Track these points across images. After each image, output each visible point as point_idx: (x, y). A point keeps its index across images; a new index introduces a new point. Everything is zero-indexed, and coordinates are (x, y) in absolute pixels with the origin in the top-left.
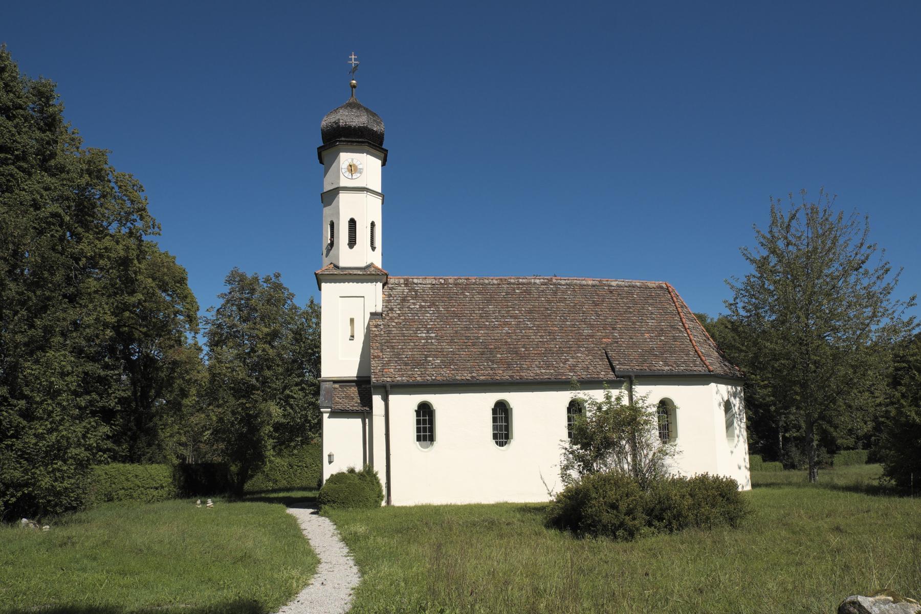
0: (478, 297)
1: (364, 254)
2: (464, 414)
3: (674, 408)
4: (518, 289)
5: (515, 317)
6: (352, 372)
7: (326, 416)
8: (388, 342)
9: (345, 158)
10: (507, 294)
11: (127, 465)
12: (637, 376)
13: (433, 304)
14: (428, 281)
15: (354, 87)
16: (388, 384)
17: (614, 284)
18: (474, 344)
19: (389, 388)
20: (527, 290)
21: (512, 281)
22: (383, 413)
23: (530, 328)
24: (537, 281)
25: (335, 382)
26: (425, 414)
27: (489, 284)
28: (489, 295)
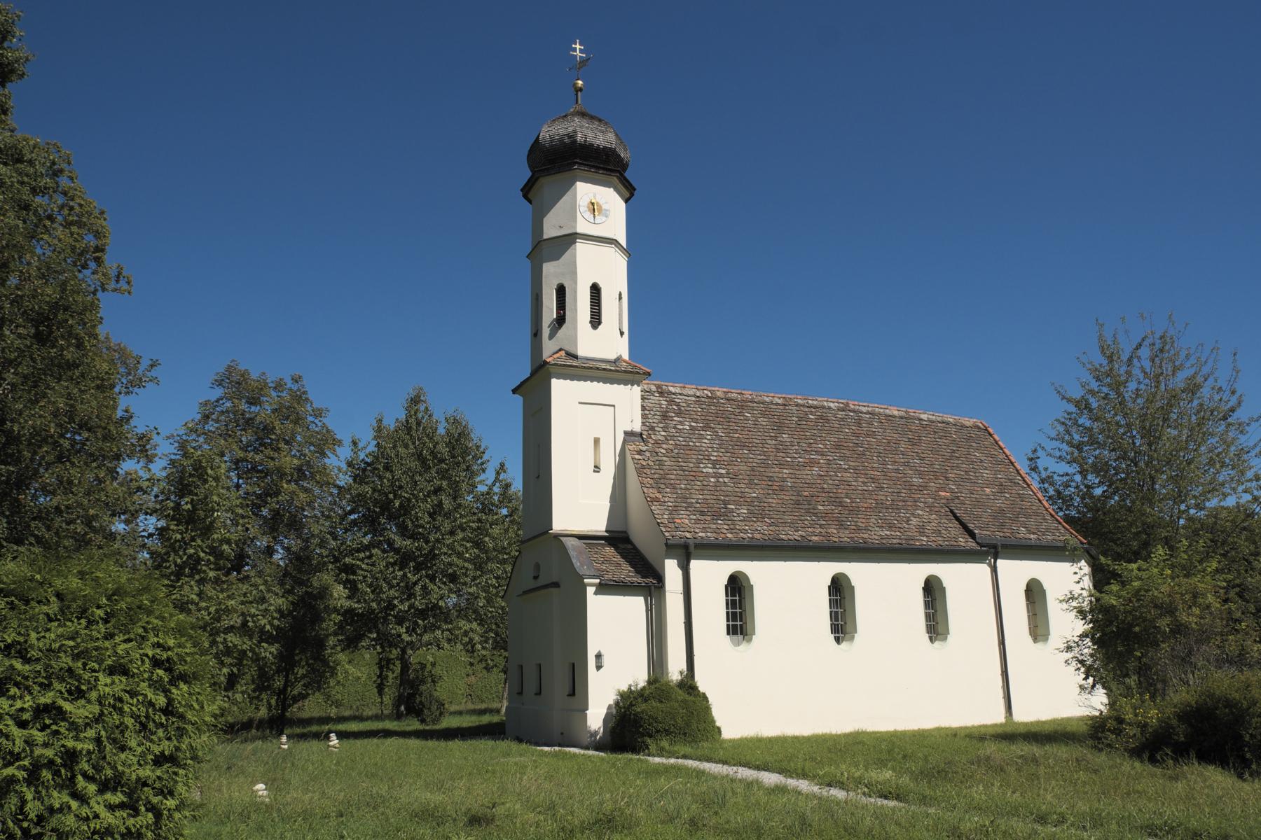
0: (763, 421)
1: (606, 341)
2: (789, 590)
3: (1043, 592)
6: (597, 523)
7: (590, 591)
9: (585, 192)
10: (800, 419)
12: (1005, 546)
15: (581, 90)
16: (691, 542)
17: (924, 417)
19: (692, 549)
20: (823, 416)
24: (832, 405)
25: (581, 537)
26: (737, 588)
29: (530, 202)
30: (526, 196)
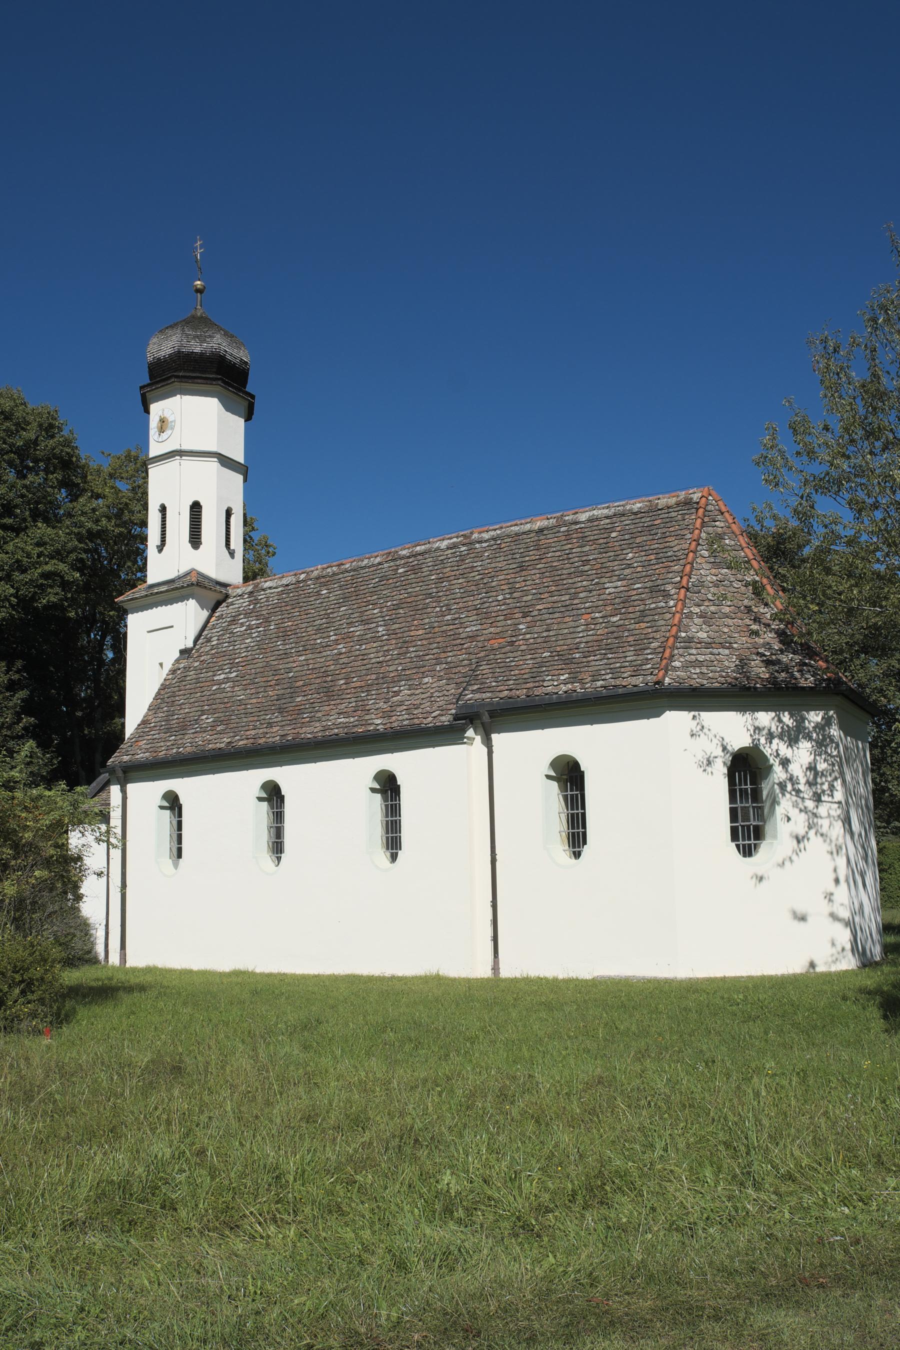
14: (285, 581)
15: (199, 291)
21: (404, 552)
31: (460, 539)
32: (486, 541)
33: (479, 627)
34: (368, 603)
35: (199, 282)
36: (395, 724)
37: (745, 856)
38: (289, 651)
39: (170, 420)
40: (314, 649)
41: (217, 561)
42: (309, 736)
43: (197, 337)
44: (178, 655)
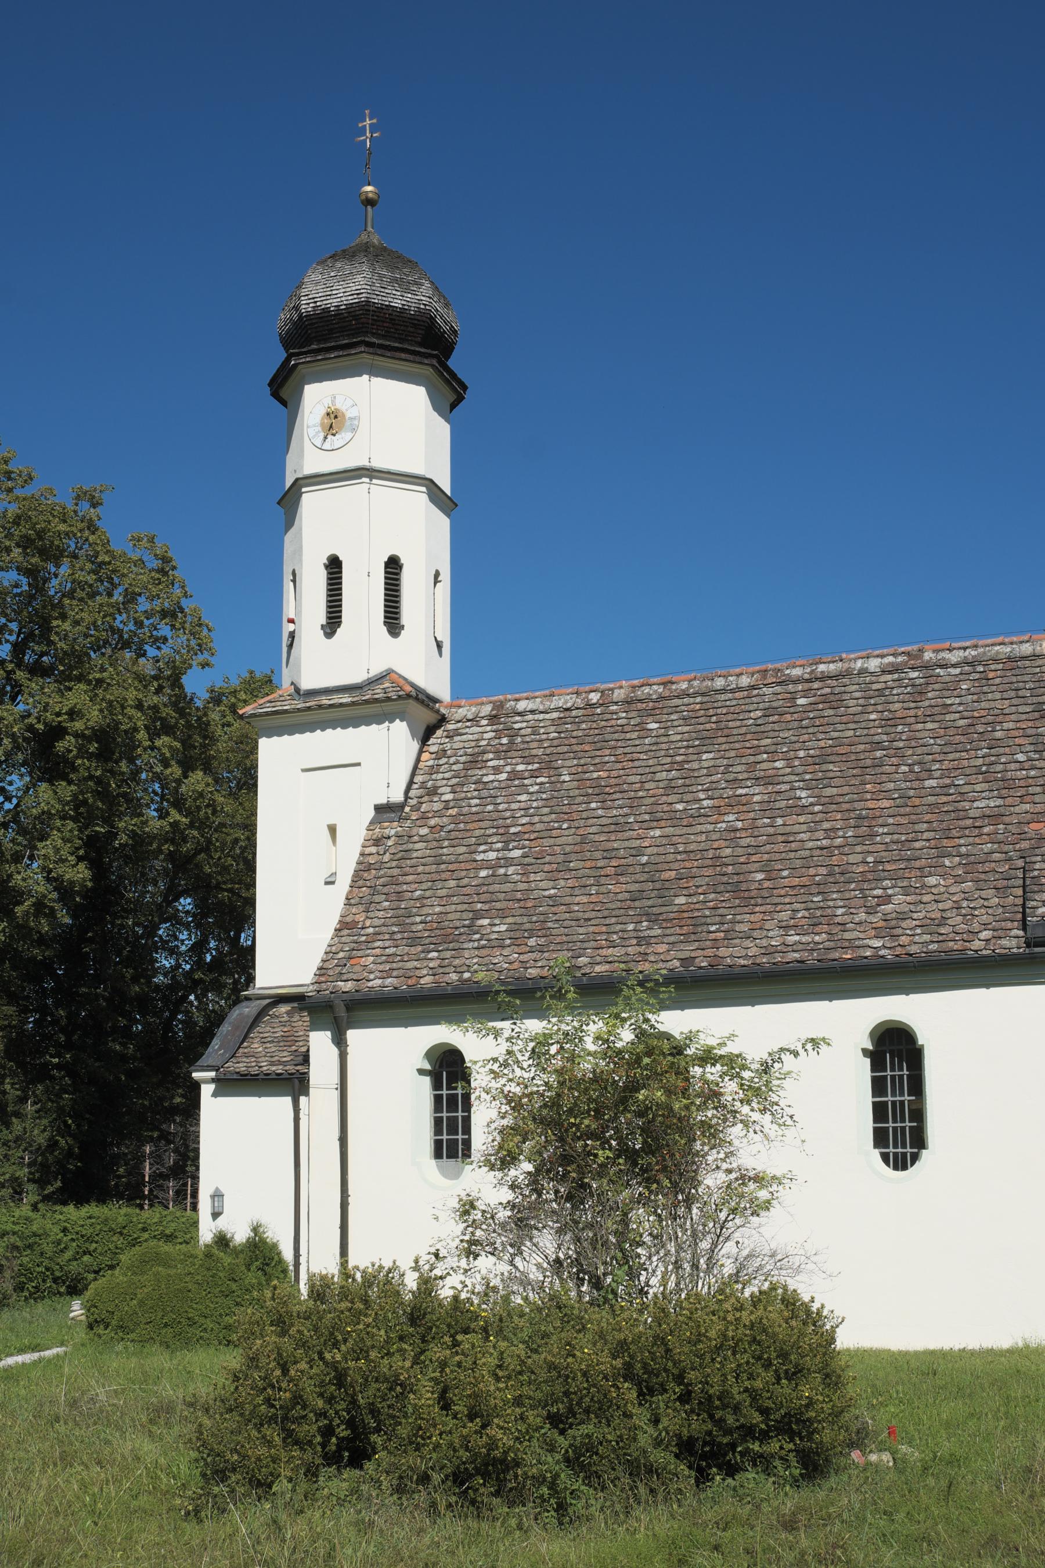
4: (805, 693)
5: (768, 781)
7: (207, 1090)
8: (394, 881)
10: (768, 712)
11: (71, 1208)
13: (548, 765)
14: (558, 702)
15: (369, 202)
18: (621, 872)
19: (342, 1012)
21: (797, 672)
22: (336, 1079)
23: (803, 810)
27: (723, 691)
28: (712, 721)
29: (284, 403)
30: (276, 395)
31: (900, 659)
32: (954, 666)
33: (999, 802)
34: (757, 750)
35: (369, 188)
36: (913, 949)
37: (896, 1168)
38: (622, 820)
39: (348, 415)
40: (674, 819)
41: (420, 659)
42: (742, 962)
43: (396, 280)
44: (372, 813)
